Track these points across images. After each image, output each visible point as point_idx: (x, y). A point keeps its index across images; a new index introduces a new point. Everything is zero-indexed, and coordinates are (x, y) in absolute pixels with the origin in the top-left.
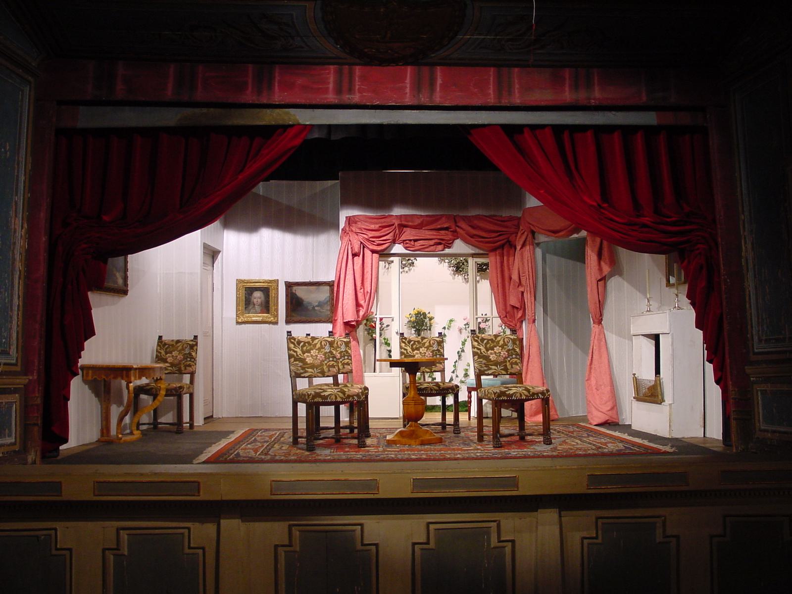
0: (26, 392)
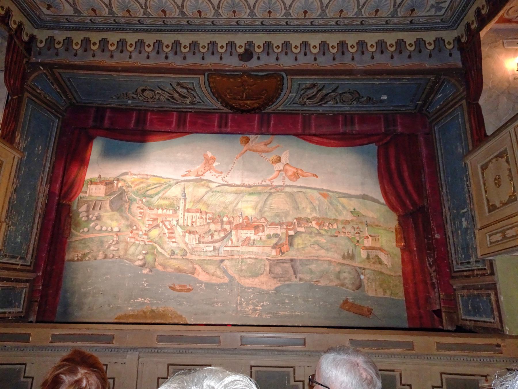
0: (33, 282)
